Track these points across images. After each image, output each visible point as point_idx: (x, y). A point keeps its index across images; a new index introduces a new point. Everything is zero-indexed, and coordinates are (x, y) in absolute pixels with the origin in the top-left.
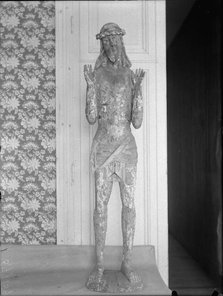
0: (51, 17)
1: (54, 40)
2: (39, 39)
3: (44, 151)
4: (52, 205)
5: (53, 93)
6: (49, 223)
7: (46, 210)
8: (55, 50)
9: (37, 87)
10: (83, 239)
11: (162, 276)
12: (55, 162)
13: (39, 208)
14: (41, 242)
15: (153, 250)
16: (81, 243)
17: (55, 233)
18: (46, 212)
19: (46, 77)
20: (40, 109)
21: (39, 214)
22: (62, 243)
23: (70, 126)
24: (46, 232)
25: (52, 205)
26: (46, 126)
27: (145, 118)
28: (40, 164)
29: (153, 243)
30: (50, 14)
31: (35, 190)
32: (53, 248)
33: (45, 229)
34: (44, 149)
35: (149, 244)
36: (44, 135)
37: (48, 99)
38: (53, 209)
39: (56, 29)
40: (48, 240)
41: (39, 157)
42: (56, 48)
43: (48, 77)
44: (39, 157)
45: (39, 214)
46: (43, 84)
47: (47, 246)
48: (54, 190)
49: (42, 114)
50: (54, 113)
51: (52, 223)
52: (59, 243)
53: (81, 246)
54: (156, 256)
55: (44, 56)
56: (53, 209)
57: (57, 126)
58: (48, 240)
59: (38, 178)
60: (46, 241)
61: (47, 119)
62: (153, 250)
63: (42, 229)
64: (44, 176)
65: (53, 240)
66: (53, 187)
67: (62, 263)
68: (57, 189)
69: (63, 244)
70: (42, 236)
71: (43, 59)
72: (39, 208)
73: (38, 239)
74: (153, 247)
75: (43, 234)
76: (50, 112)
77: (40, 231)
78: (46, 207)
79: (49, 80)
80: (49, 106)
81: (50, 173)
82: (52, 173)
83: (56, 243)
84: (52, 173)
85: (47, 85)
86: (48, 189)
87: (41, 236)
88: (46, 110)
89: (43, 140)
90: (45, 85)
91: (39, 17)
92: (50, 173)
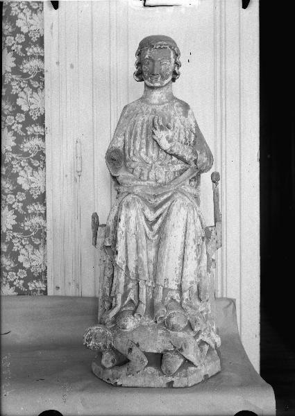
1: (42, 58)
2: (13, 56)
3: (23, 116)
4: (37, 220)
6: (32, 176)
8: (44, 155)
12: (43, 137)
13: (13, 226)
15: (232, 306)
18: (28, 233)
19: (27, 128)
20: (14, 193)
21: (14, 237)
22: (60, 293)
23: (72, 66)
24: (28, 271)
28: (16, 220)
30: (35, 7)
33: (26, 265)
34: (22, 112)
35: (224, 296)
36: (23, 241)
37: (30, 171)
38: (40, 227)
39: (47, 195)
40: (31, 286)
45: (14, 237)
46: (21, 64)
48: (43, 192)
49: (18, 44)
50: (41, 42)
51: (39, 253)
52: (50, 293)
55: (22, 89)
56: (40, 227)
57: (49, 66)
58: (31, 286)
59: (13, 246)
61: (29, 54)
62: (232, 306)
64: (22, 84)
65: (40, 285)
66: (41, 185)
71: (21, 15)
72: (13, 226)
73: (11, 284)
74: (232, 301)
76: (34, 39)
78: (27, 225)
79: (33, 56)
80: (32, 107)
81: (35, 158)
82: (37, 158)
83: (45, 293)
84: (37, 158)
86: (31, 267)
87: (17, 278)
88: (26, 35)
89: (21, 94)
90: (25, 145)
92: (35, 158)
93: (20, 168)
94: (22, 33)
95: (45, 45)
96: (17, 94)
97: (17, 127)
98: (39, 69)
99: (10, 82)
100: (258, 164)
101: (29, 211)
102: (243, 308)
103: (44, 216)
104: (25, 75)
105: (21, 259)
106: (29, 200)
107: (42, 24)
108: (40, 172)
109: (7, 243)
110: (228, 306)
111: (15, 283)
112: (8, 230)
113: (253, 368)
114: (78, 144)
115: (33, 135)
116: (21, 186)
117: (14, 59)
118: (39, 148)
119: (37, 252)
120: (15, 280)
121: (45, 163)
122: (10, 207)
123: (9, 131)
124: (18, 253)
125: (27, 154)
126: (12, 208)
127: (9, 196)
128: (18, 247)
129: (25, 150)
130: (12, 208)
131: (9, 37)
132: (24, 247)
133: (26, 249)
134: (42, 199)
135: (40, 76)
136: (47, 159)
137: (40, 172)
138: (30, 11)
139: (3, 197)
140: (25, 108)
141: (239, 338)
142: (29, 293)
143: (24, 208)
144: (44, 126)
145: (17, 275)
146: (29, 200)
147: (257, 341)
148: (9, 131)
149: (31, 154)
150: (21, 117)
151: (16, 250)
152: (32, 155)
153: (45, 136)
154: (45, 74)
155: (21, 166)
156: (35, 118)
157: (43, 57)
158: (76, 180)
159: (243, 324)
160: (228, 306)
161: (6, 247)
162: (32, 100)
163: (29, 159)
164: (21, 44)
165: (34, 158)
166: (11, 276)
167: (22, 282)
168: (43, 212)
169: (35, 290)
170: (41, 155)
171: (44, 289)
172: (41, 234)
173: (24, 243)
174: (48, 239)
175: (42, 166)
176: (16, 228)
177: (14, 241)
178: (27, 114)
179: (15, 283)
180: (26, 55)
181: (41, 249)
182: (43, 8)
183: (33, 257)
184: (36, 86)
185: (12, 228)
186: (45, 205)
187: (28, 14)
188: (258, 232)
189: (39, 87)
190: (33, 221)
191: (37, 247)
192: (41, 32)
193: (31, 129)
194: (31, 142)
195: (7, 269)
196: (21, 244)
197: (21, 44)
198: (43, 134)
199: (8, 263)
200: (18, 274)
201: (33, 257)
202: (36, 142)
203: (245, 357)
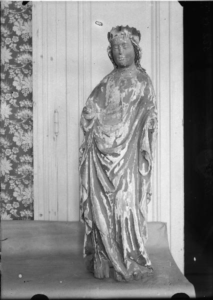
0: (27, 21)
1: (31, 53)
3: (17, 94)
4: (27, 167)
5: (29, 125)
7: (19, 173)
8: (32, 121)
9: (7, 117)
10: (69, 211)
11: (179, 267)
12: (31, 109)
14: (12, 216)
15: (164, 229)
16: (68, 218)
17: (32, 204)
18: (20, 176)
20: (11, 147)
21: (10, 179)
22: (42, 219)
24: (20, 203)
25: (27, 167)
26: (20, 114)
27: (155, 172)
28: (12, 111)
29: (165, 219)
30: (26, 18)
31: (5, 147)
32: (28, 225)
33: (19, 199)
35: (159, 221)
36: (17, 182)
37: (22, 22)
38: (29, 172)
40: (23, 214)
41: (10, 46)
42: (34, 119)
43: (22, 48)
44: (10, 102)
45: (10, 179)
47: (20, 221)
48: (31, 147)
49: (14, 43)
50: (30, 42)
51: (28, 190)
52: (35, 218)
53: (67, 222)
54: (169, 235)
56: (29, 172)
57: (35, 58)
58: (23, 214)
60: (19, 215)
63: (15, 199)
65: (28, 213)
67: (43, 245)
68: (34, 144)
69: (43, 220)
70: (14, 209)
71: (16, 23)
72: (10, 171)
73: (8, 213)
74: (165, 224)
75: (16, 205)
76: (25, 40)
77: (11, 202)
78: (20, 170)
79: (24, 52)
81: (25, 68)
83: (32, 218)
85: (20, 114)
87: (12, 208)
88: (20, 37)
90: (19, 114)
91: (11, 77)
93: (15, 75)
94: (17, 35)
95: (33, 44)
96: (13, 134)
97: (13, 46)
98: (28, 61)
99: (8, 181)
100: (182, 128)
101: (21, 161)
102: (172, 229)
103: (32, 164)
104: (19, 65)
105: (15, 194)
106: (21, 42)
107: (31, 30)
108: (29, 133)
109: (5, 17)
110: (162, 227)
111: (11, 212)
112: (5, 8)
113: (179, 270)
114: (56, 114)
115: (24, 107)
116: (16, 198)
117: (11, 53)
118: (28, 116)
119: (26, 190)
120: (10, 100)
121: (32, 126)
122: (8, 47)
123: (7, 160)
124: (13, 191)
125: (20, 120)
126: (9, 48)
127: (7, 150)
128: (12, 20)
129: (19, 118)
130: (9, 48)
131: (8, 150)
132: (17, 186)
133: (19, 22)
134: (30, 152)
135: (29, 65)
136: (33, 12)
137: (29, 133)
138: (23, 20)
139: (3, 39)
140: (18, 88)
141: (169, 251)
142: (20, 218)
143: (18, 158)
144: (32, 101)
145: (11, 96)
146: (21, 153)
147: (182, 253)
148: (7, 160)
149: (22, 10)
150: (16, 39)
151: (11, 22)
152: (23, 11)
153: (33, 162)
154: (33, 64)
155: (15, 73)
156: (25, 95)
157: (32, 52)
158: (54, 138)
159: (172, 240)
160: (162, 227)
161: (4, 186)
162: (24, 82)
163: (21, 13)
164: (16, 43)
165: (24, 123)
166: (7, 41)
167: (16, 211)
168: (31, 161)
169: (25, 217)
170: (29, 121)
171: (31, 216)
172: (30, 177)
173: (16, 18)
174: (34, 180)
175: (30, 129)
176: (12, 62)
177: (10, 71)
178: (20, 93)
179: (11, 212)
180: (20, 51)
181: (29, 188)
182: (31, 18)
183: (24, 193)
184: (26, 73)
185: (8, 7)
186: (32, 156)
187: (21, 22)
188: (183, 175)
189: (28, 18)
190: (24, 167)
191: (26, 186)
192: (30, 90)
193: (23, 159)
194: (23, 112)
195: (5, 35)
196: (16, 184)
197: (16, 43)
198: (31, 106)
199: (6, 31)
200: (13, 95)
201: (24, 193)
202: (26, 112)
203: (174, 264)
